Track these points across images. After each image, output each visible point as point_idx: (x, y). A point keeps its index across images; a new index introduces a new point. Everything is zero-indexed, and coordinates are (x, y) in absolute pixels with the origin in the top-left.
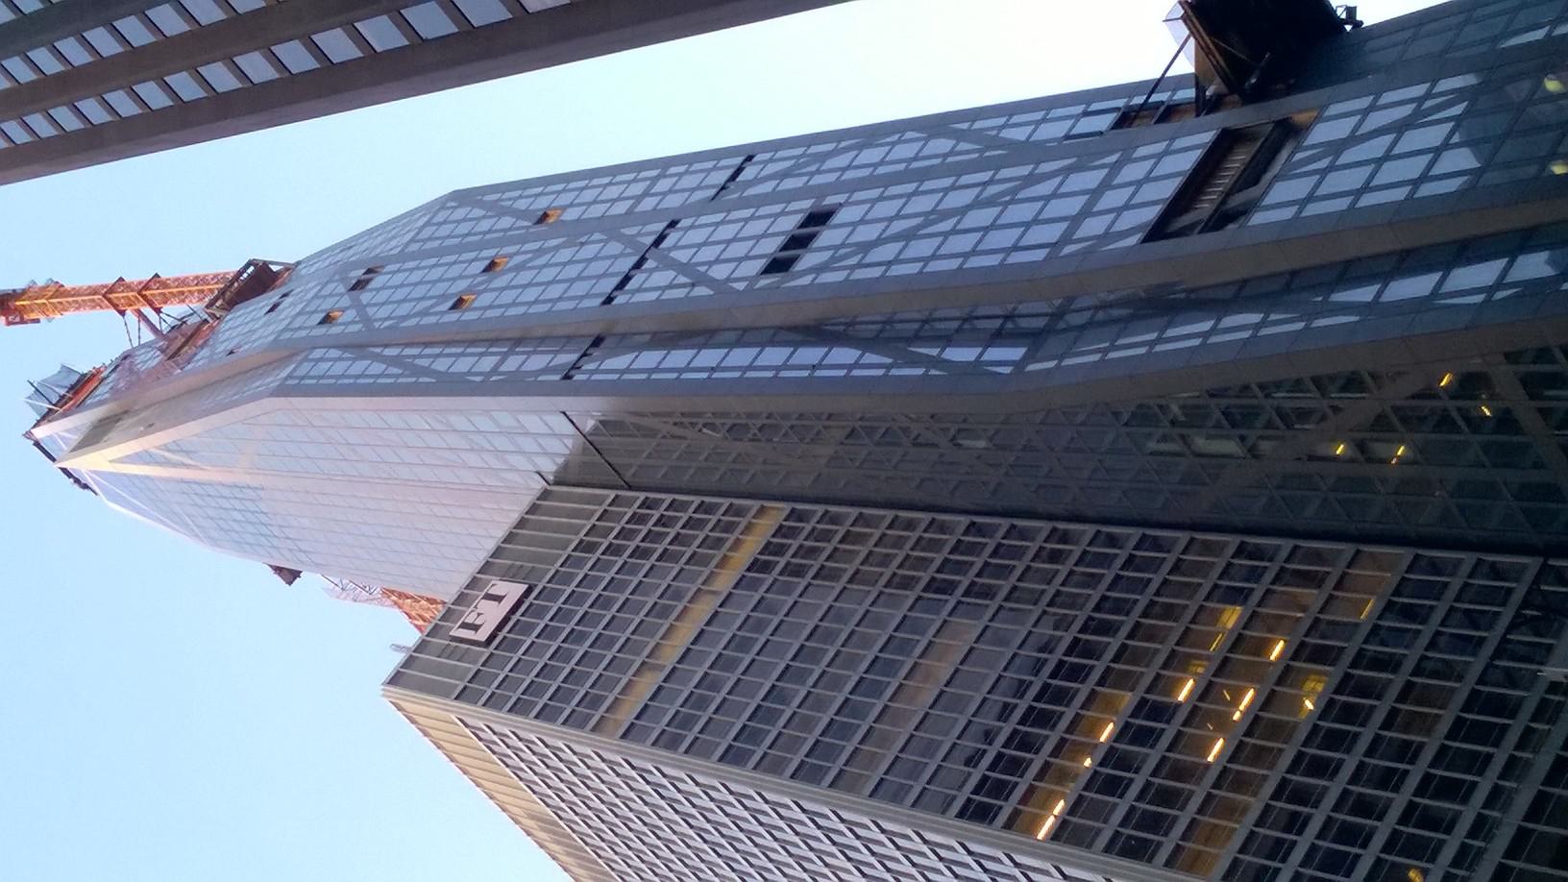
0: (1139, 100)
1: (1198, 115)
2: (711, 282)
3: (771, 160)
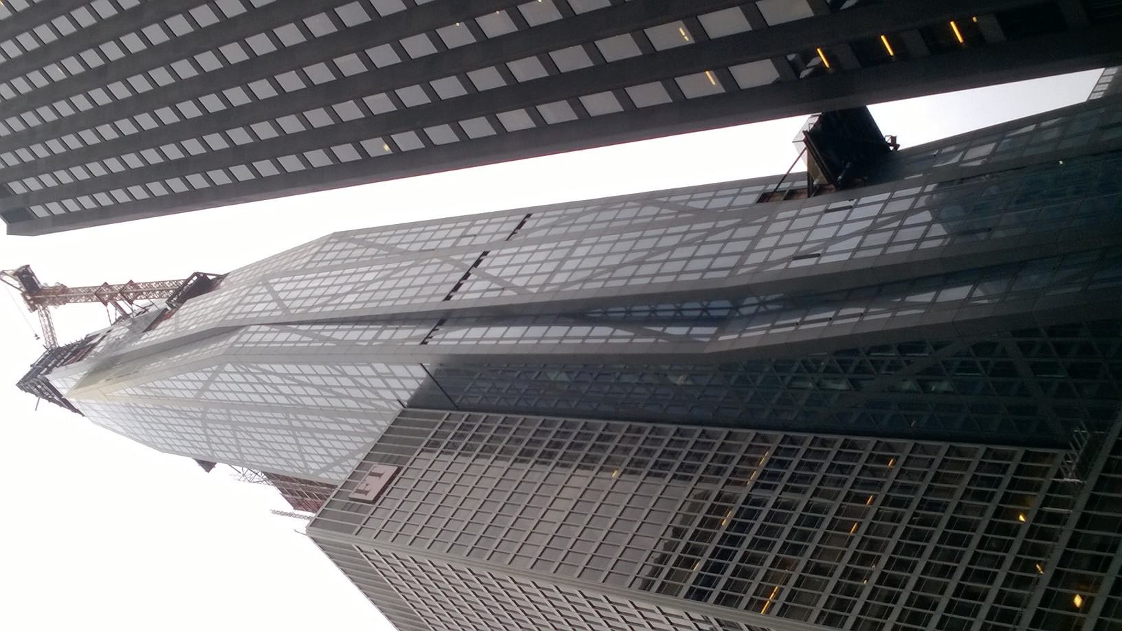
0: (772, 187)
1: (809, 197)
2: (513, 288)
3: (542, 217)
